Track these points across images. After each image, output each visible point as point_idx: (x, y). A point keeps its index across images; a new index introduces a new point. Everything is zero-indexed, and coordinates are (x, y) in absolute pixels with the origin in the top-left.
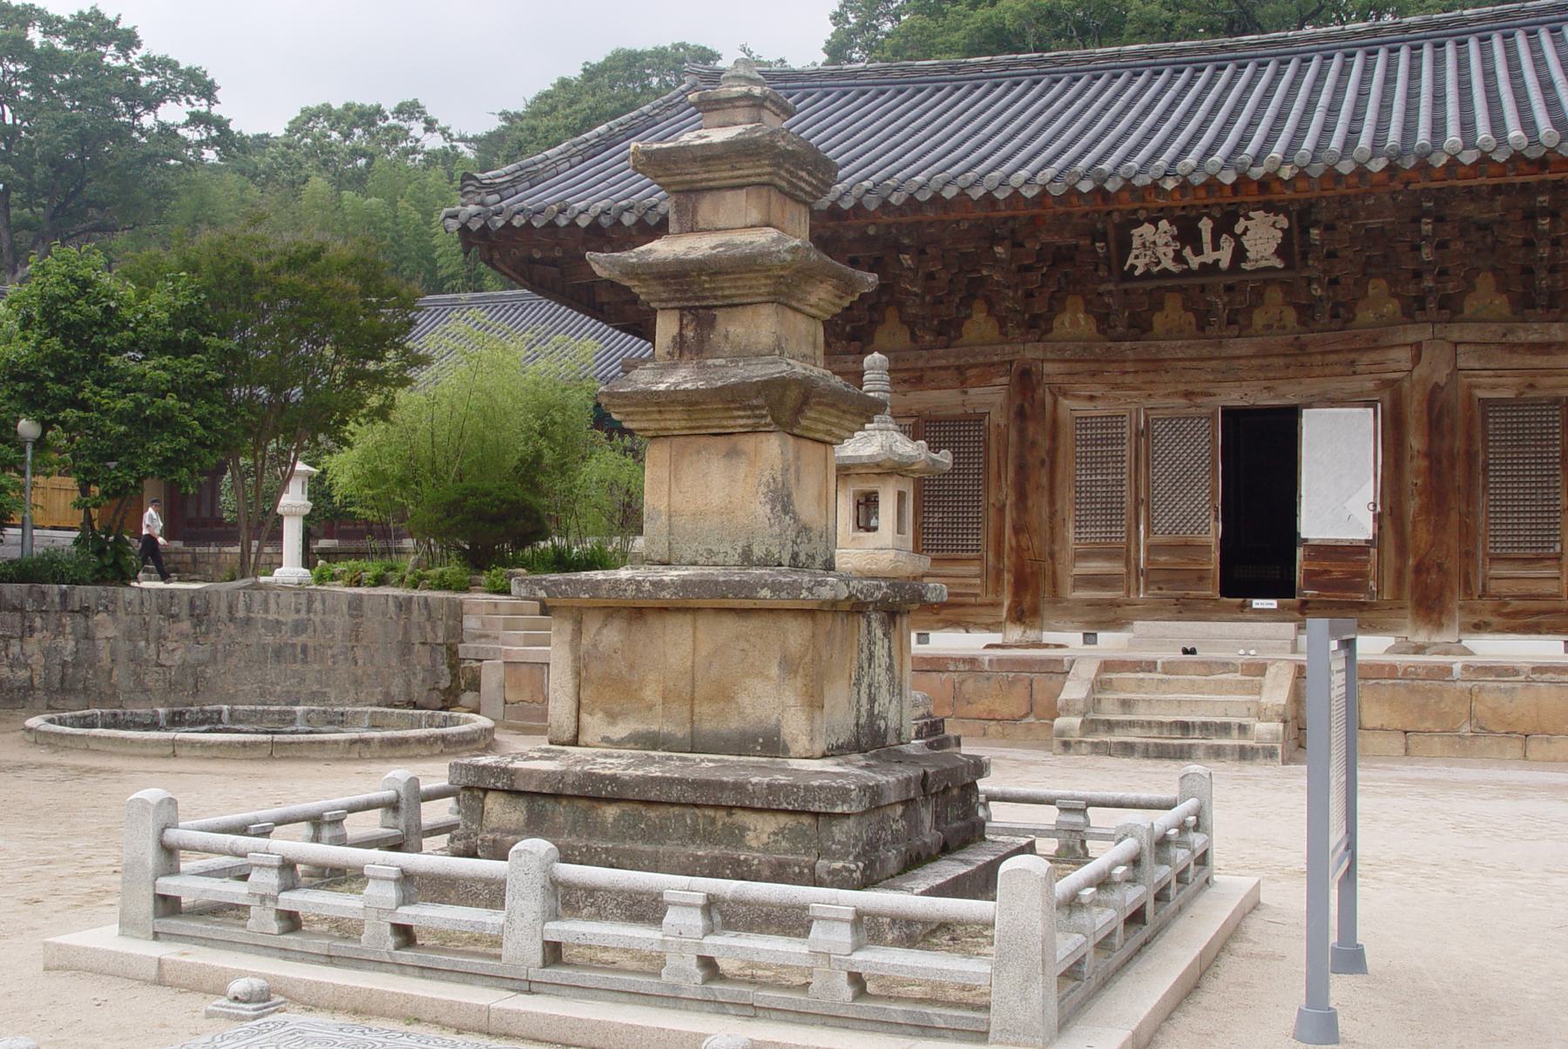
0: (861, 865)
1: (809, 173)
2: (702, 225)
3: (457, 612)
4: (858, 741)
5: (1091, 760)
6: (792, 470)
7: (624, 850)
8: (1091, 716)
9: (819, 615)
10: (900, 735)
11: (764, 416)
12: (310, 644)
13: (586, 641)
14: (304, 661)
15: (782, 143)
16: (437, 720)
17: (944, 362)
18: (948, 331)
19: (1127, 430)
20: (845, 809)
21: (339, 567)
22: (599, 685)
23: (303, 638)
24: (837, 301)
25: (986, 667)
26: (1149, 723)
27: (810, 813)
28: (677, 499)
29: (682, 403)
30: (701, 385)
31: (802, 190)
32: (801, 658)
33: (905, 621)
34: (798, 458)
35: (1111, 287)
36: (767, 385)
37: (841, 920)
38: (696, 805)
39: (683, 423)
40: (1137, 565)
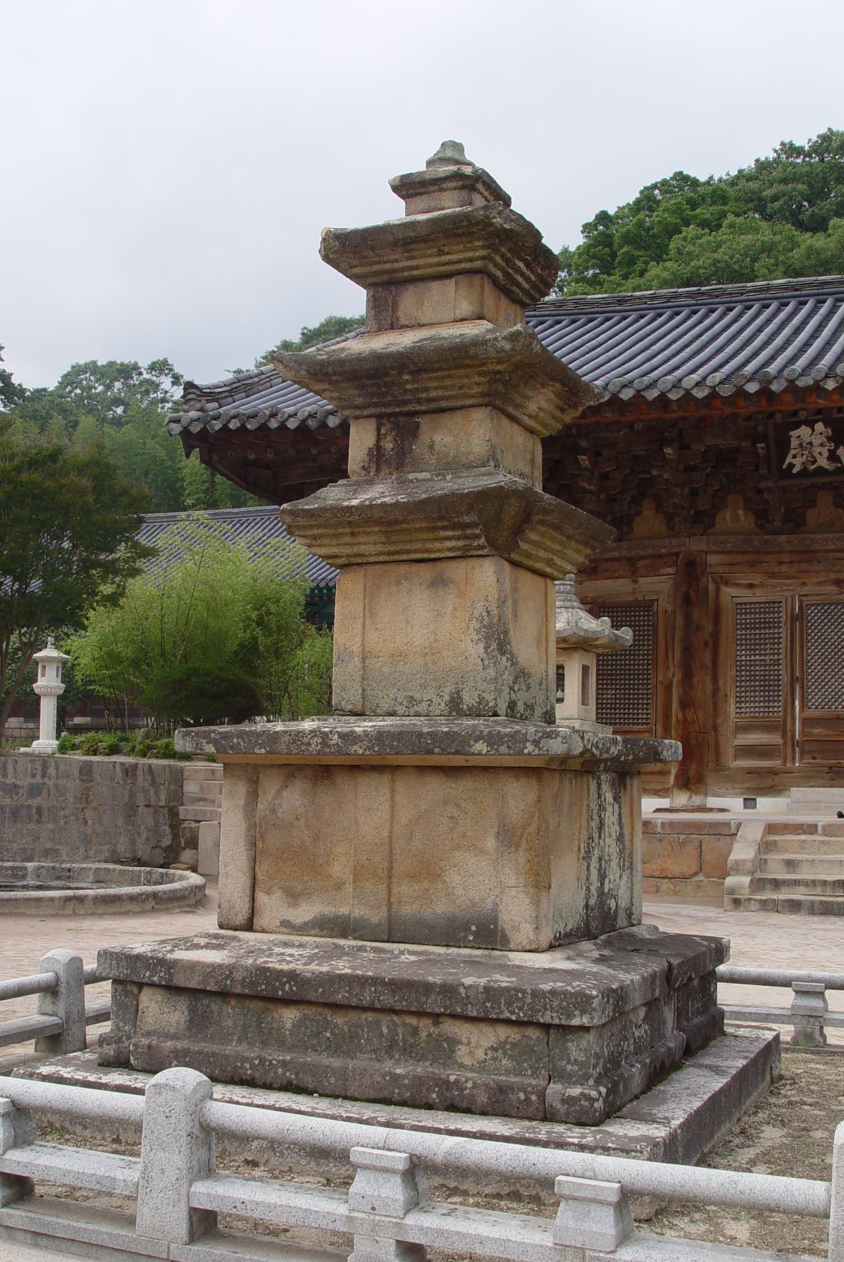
0: (603, 1090)
1: (528, 265)
2: (403, 321)
3: (178, 778)
4: (587, 925)
5: (761, 916)
6: (509, 603)
7: (304, 1064)
8: (759, 875)
9: (546, 775)
10: (630, 915)
11: (477, 537)
12: (44, 805)
13: (262, 806)
14: (39, 821)
15: (498, 220)
16: (155, 877)
17: (617, 554)
18: (623, 524)
19: (783, 615)
20: (585, 1020)
21: (79, 739)
22: (277, 859)
23: (35, 802)
24: (558, 414)
25: (659, 829)
26: (814, 881)
27: (539, 1025)
28: (373, 638)
29: (379, 522)
30: (402, 498)
31: (519, 286)
32: (524, 827)
33: (635, 784)
34: (515, 590)
35: (770, 484)
36: (483, 495)
37: (601, 1202)
38: (393, 1011)
39: (380, 548)
40: (793, 735)
